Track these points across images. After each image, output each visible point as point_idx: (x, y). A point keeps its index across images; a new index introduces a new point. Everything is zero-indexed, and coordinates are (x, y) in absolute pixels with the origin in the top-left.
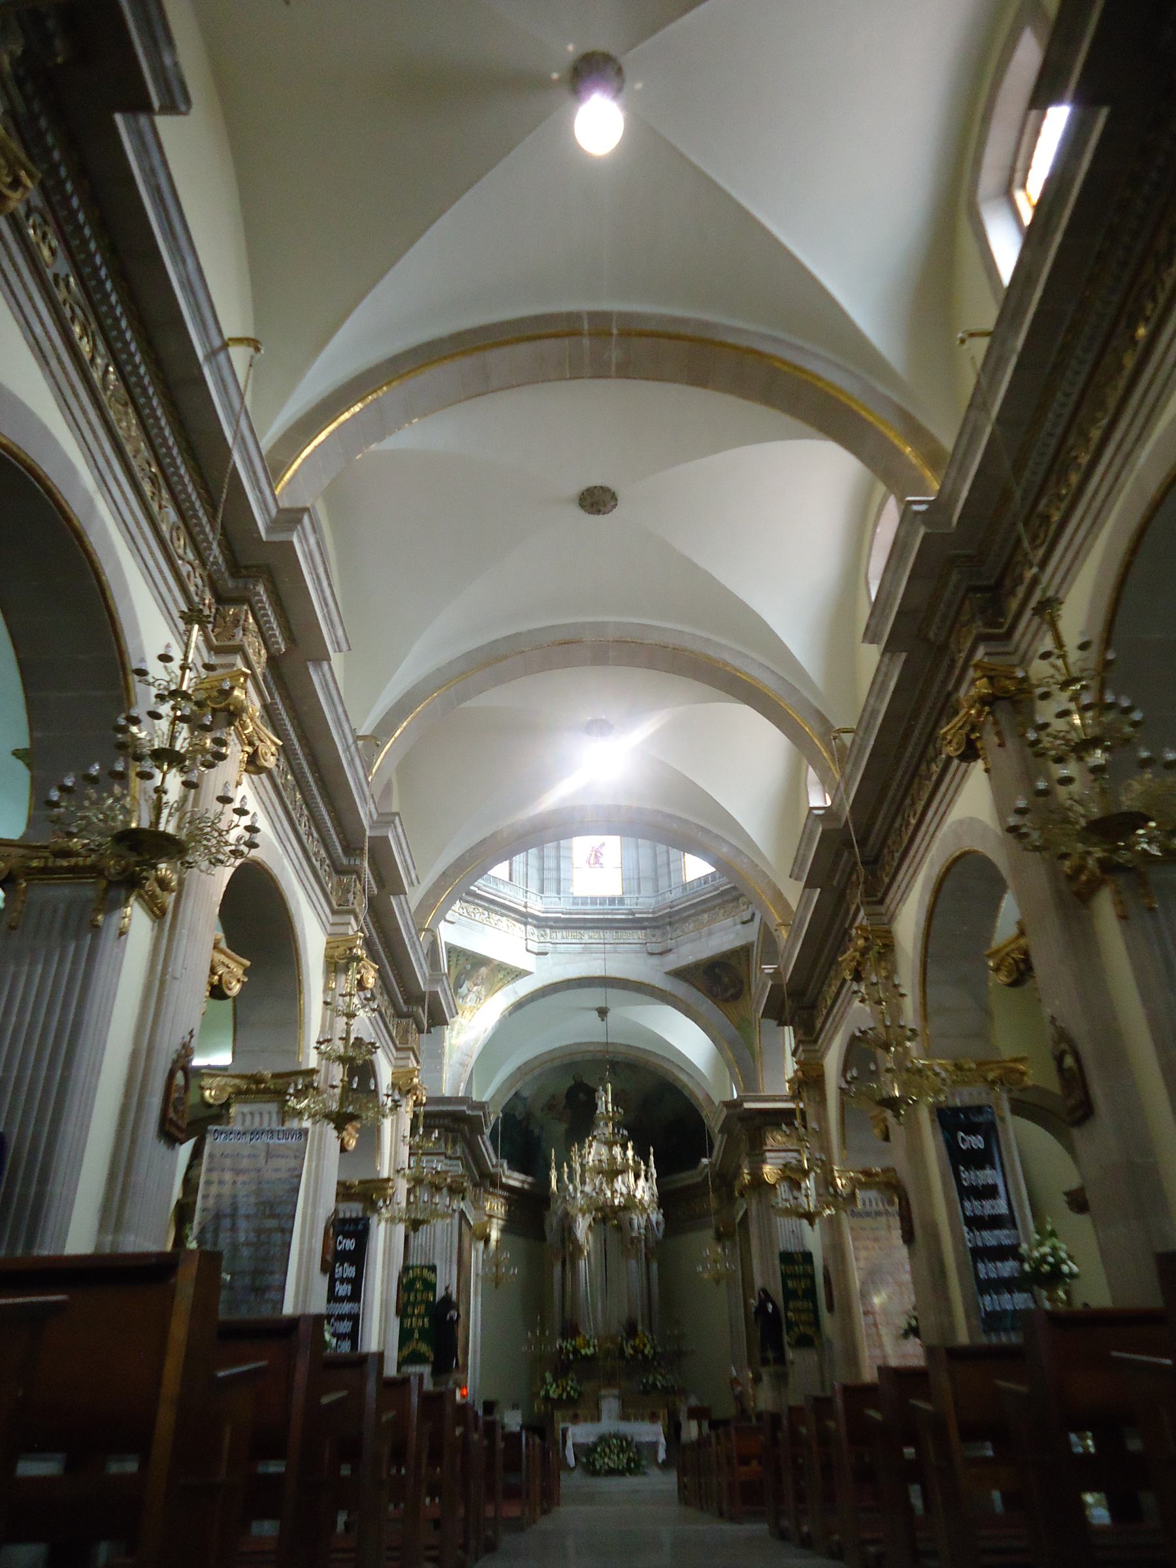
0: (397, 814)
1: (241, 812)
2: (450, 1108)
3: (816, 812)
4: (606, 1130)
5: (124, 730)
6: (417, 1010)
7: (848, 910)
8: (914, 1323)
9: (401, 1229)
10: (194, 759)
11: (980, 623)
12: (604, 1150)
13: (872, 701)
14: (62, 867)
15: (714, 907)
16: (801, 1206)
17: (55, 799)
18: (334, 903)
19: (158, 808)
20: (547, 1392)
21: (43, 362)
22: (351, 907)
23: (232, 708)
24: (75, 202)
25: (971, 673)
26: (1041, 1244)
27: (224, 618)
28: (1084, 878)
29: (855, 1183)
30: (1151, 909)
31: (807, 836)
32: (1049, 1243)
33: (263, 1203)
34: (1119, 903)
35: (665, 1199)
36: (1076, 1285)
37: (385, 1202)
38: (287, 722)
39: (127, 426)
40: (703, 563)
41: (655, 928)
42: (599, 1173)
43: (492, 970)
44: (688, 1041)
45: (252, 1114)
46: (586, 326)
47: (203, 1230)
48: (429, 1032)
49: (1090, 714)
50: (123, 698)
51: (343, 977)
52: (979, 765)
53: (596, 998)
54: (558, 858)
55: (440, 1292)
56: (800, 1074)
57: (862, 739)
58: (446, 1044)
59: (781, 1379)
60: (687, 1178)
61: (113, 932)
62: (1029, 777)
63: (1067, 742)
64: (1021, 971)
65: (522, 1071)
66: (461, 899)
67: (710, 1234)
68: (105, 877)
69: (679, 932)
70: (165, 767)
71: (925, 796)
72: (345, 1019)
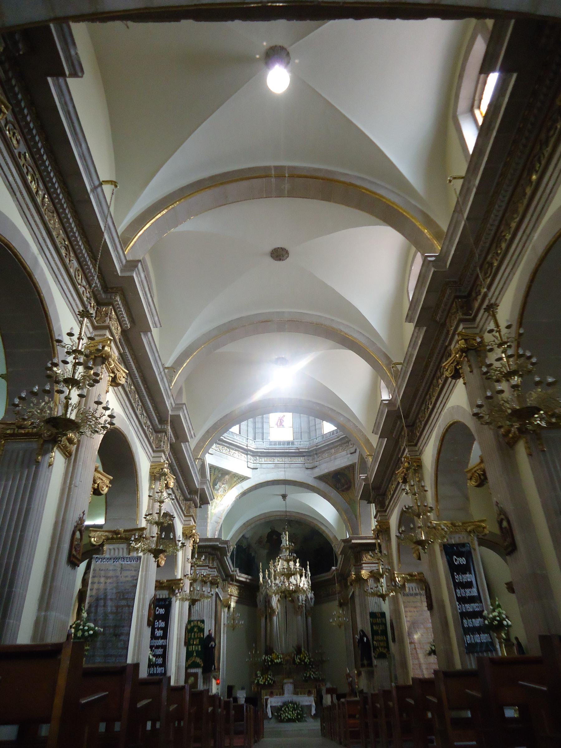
0: (185, 404)
1: (106, 408)
2: (211, 544)
3: (384, 402)
4: (285, 554)
5: (51, 369)
6: (194, 497)
7: (400, 449)
8: (433, 648)
9: (187, 604)
10: (84, 383)
11: (460, 314)
12: (285, 563)
13: (410, 349)
14: (22, 433)
15: (337, 446)
16: (379, 591)
17: (17, 403)
18: (154, 447)
19: (66, 406)
20: (258, 681)
21: (13, 194)
22: (162, 449)
23: (104, 356)
24: (29, 119)
25: (456, 337)
26: (494, 611)
27: (101, 313)
28: (511, 435)
29: (405, 580)
30: (544, 451)
31: (380, 413)
32: (497, 610)
33: (119, 592)
34: (528, 448)
35: (314, 586)
36: (511, 630)
37: (179, 590)
38: (131, 361)
39: (54, 223)
40: (329, 284)
41: (310, 456)
42: (283, 575)
43: (231, 477)
44: (325, 510)
45: (114, 549)
46: (273, 172)
47: (90, 607)
48: (200, 507)
49: (511, 359)
50: (52, 353)
51: (158, 483)
52: (461, 381)
53: (281, 490)
54: (263, 423)
55: (206, 633)
56: (378, 527)
57: (406, 367)
58: (209, 513)
59: (371, 674)
60: (325, 576)
61: (46, 464)
62: (484, 388)
63: (501, 372)
64: (482, 480)
65: (245, 525)
66: (216, 443)
67: (337, 603)
68: (42, 438)
69: (320, 458)
70: (70, 387)
71: (436, 395)
72: (159, 504)
